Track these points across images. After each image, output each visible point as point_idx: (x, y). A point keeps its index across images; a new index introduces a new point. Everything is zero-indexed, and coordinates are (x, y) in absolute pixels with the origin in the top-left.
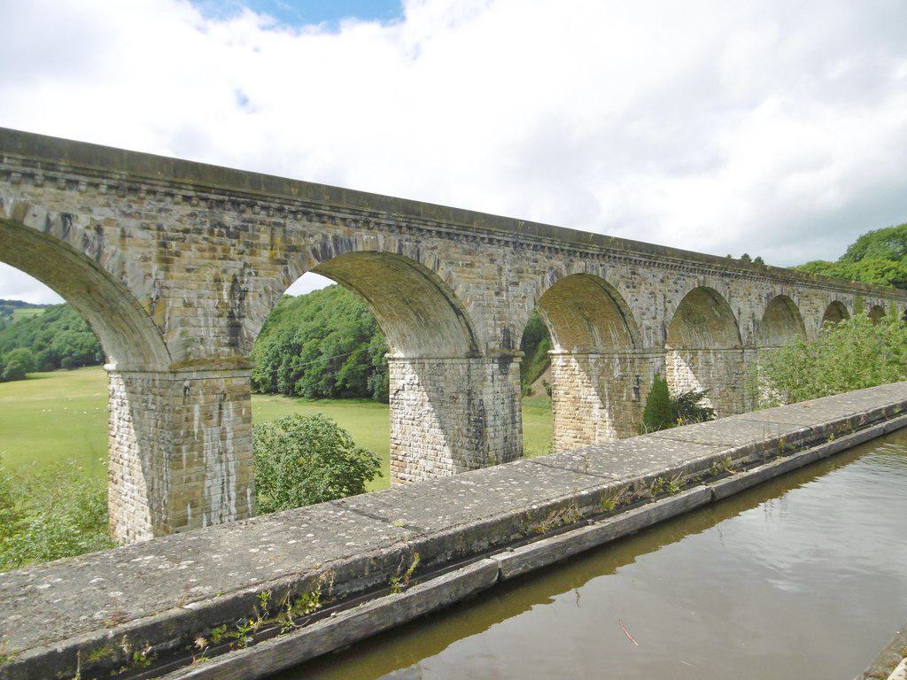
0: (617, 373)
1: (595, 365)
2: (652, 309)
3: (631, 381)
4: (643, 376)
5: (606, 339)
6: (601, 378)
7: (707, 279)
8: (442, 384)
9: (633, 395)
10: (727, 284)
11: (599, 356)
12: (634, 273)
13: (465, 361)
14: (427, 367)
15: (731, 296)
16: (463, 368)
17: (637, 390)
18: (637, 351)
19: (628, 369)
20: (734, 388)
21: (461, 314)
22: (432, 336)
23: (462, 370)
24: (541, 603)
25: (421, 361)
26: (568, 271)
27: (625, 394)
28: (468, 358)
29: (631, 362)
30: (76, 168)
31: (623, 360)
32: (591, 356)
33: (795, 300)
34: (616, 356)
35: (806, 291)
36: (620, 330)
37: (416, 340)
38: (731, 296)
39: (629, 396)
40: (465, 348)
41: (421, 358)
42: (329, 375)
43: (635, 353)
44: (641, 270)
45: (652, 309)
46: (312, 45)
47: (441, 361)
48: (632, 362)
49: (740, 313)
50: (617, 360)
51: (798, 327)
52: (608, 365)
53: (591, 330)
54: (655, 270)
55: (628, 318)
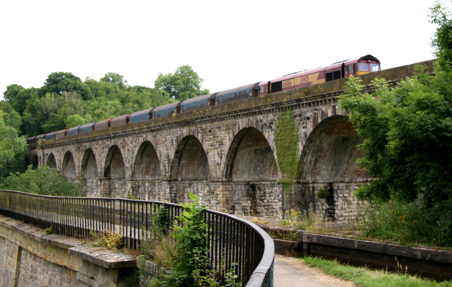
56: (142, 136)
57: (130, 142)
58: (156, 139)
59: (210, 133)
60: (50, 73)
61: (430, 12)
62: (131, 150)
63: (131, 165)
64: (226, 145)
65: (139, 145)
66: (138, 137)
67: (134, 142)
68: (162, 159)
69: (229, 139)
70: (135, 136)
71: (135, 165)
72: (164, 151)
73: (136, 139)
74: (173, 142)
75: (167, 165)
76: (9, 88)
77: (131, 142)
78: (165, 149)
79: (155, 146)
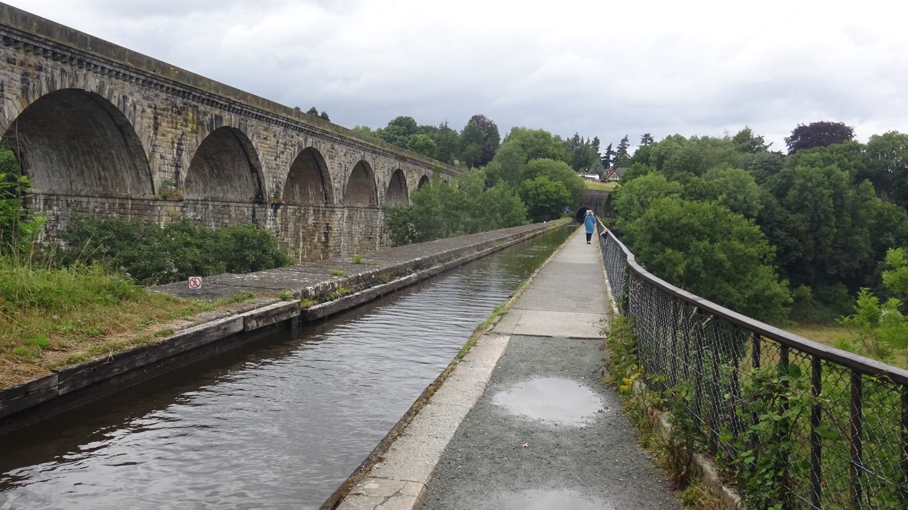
0: (311, 221)
1: (293, 214)
2: (339, 175)
3: (322, 228)
4: (332, 224)
5: (304, 195)
6: (297, 224)
7: (366, 154)
8: (227, 221)
9: (323, 238)
10: (374, 159)
11: (296, 207)
12: (333, 148)
13: (251, 205)
14: (211, 207)
15: (375, 169)
16: (248, 211)
17: (326, 235)
18: (329, 205)
19: (321, 218)
20: (370, 238)
21: (257, 172)
22: (220, 184)
23: (248, 212)
24: (94, 441)
25: (204, 202)
26: (305, 145)
27: (316, 237)
28: (254, 203)
29: (323, 213)
30: (166, 79)
31: (316, 212)
32: (289, 207)
33: (405, 173)
34: (311, 208)
35: (411, 166)
36: (317, 188)
37: (202, 186)
38: (375, 169)
39: (319, 239)
40: (251, 195)
41: (206, 200)
42: (818, 200)
43: (327, 207)
44: (336, 146)
45: (339, 175)
46: (817, 120)
47: (226, 204)
48: (324, 214)
49: (378, 182)
50: (312, 211)
51: (404, 194)
52: (304, 214)
53: (292, 187)
54: (343, 146)
55: (326, 180)
56: (360, 153)
57: (343, 154)
62: (343, 166)
63: (344, 186)
65: (356, 164)
66: (354, 151)
67: (349, 155)
73: (352, 154)
75: (383, 193)
77: (345, 155)
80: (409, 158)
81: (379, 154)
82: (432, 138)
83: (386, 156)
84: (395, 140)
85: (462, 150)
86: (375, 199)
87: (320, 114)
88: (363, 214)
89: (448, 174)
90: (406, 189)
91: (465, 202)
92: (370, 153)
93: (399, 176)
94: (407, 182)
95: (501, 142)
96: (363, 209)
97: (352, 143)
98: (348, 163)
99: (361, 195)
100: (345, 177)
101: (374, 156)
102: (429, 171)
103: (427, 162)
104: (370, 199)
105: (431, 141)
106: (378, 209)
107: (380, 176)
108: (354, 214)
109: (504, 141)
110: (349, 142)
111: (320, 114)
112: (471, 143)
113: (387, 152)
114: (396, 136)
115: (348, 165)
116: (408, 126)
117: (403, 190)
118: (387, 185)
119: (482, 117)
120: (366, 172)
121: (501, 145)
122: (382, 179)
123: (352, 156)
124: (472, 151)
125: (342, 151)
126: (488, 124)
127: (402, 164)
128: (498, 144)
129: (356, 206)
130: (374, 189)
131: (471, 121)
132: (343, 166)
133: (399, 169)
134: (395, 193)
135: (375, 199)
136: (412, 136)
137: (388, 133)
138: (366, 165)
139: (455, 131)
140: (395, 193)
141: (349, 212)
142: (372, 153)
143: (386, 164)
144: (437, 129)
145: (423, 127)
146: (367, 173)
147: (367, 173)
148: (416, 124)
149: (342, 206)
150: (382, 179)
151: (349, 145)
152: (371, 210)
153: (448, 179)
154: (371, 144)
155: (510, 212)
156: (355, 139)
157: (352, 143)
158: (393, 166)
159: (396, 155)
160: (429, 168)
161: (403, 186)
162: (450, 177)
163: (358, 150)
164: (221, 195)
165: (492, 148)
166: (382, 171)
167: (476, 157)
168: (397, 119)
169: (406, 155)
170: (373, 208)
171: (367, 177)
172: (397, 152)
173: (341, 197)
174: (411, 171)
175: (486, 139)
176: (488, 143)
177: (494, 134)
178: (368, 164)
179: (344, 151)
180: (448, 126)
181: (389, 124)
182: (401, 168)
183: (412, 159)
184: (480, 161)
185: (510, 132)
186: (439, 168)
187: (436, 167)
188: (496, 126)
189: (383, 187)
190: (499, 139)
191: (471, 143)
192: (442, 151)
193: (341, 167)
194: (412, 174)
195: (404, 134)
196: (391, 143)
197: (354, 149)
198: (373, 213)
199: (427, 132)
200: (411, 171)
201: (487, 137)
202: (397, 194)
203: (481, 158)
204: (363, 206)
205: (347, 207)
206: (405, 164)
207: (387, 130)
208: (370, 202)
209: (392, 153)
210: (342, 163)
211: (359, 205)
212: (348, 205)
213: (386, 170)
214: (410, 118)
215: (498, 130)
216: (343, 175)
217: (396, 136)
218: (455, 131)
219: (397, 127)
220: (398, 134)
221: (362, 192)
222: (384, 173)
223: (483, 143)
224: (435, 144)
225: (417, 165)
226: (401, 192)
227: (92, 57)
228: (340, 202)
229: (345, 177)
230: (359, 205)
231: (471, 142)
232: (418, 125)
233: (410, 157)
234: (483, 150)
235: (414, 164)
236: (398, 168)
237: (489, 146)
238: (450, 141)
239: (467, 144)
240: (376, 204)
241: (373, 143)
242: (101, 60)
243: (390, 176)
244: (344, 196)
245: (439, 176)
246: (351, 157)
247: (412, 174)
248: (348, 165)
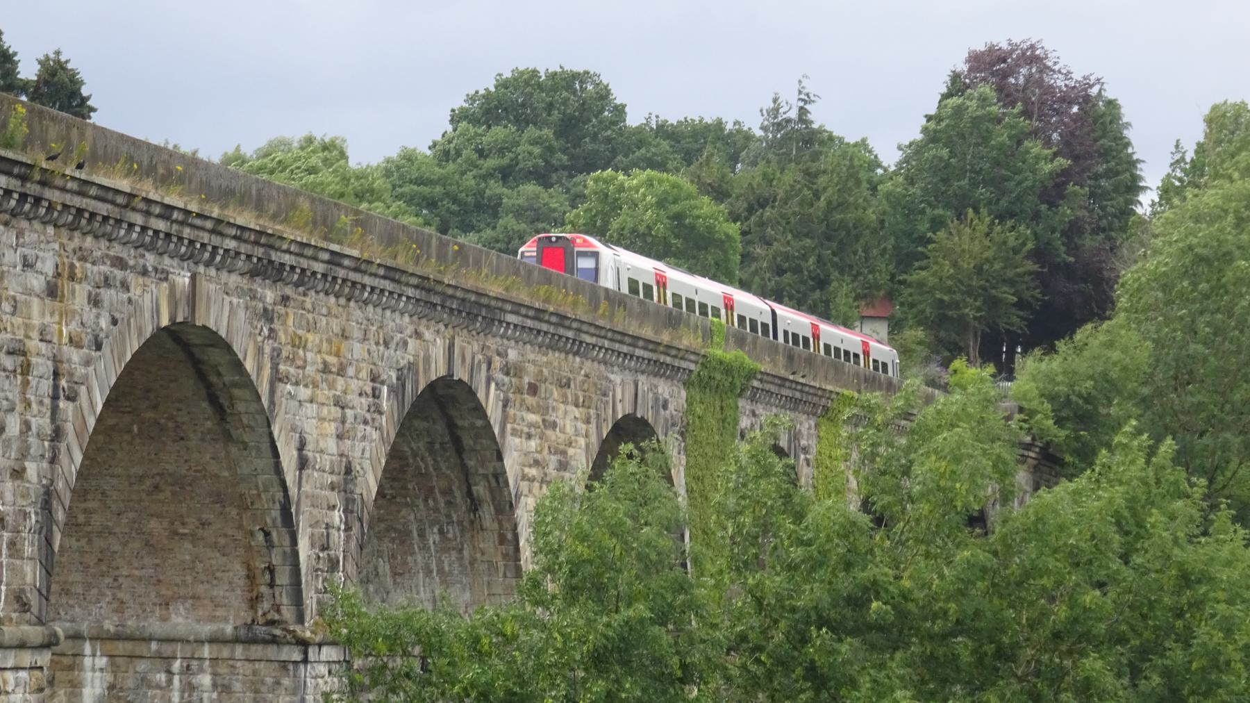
10: (267, 316)
15: (277, 378)
38: (277, 378)
49: (303, 464)
51: (488, 543)
54: (32, 233)
56: (164, 276)
57: (37, 283)
58: (272, 333)
59: (530, 400)
60: (1219, 100)
61: (924, 121)
62: (42, 366)
63: (47, 498)
64: (993, 533)
65: (133, 345)
66: (120, 263)
67: (81, 291)
68: (306, 488)
69: (587, 445)
70: (99, 248)
71: (80, 493)
72: (324, 436)
73: (107, 282)
74: (376, 395)
75: (338, 537)
76: (1215, 108)
77: (52, 291)
78: (331, 428)
79: (264, 390)
80: (517, 307)
81: (305, 280)
82: (719, 193)
83: (351, 292)
84: (492, 209)
85: (906, 260)
86: (283, 578)
87: (28, 70)
88: (206, 680)
89: (794, 404)
90: (505, 508)
91: (874, 589)
92: (234, 280)
93: (451, 426)
94: (511, 463)
95: (1146, 202)
96: (206, 651)
97: (103, 209)
98: (74, 342)
99: (185, 552)
100: (57, 435)
101: (270, 295)
102: (664, 388)
103: (647, 332)
104: (251, 577)
105: (706, 206)
106: (304, 644)
107: (310, 428)
108: (144, 682)
109: (1167, 191)
110: (78, 201)
111: (28, 70)
112: (960, 216)
113: (360, 266)
114: (495, 188)
115: (75, 356)
116: (570, 127)
117: (487, 514)
118: (368, 484)
119: (1032, 57)
120: (213, 399)
121: (1142, 222)
122: (331, 445)
123: (108, 295)
124: (967, 264)
125: (27, 264)
126: (1066, 100)
127: (469, 346)
128: (1126, 212)
129: (155, 626)
130: (276, 513)
131: (957, 85)
132: (42, 366)
133: (447, 382)
134: (433, 537)
135: (283, 578)
136: (590, 182)
137: (451, 166)
138: (215, 356)
139: (863, 144)
140: (433, 537)
141: (114, 667)
142: (253, 274)
143: (358, 350)
144: (748, 137)
145: (664, 131)
146: (221, 412)
147: (221, 412)
148: (620, 111)
149: (35, 633)
150: (325, 446)
151: (79, 221)
152: (257, 651)
153: (795, 436)
154: (245, 218)
155: (1185, 639)
156: (124, 185)
157: (103, 209)
158: (405, 359)
159: (424, 284)
160: (659, 370)
161: (480, 490)
162: (806, 425)
163: (150, 259)
164: (257, 666)
165: (1089, 242)
166: (324, 393)
167: (993, 303)
168: (503, 85)
169: (495, 289)
170: (274, 640)
171: (228, 438)
172: (429, 269)
173: (31, 573)
174: (533, 389)
175: (1054, 191)
176: (1067, 212)
177: (1105, 154)
178: (228, 348)
179: (49, 268)
180: (820, 117)
181: (457, 117)
182: (461, 374)
183: (539, 314)
184: (1016, 321)
185: (1194, 134)
186: (728, 369)
187: (705, 362)
188: (1111, 104)
189: (335, 498)
190: (1133, 187)
191: (960, 216)
192: (780, 272)
193: (26, 369)
194: (543, 410)
195: (542, 177)
196: (467, 228)
197: (117, 250)
198: (268, 673)
199: (689, 157)
200: (533, 389)
201: (1064, 176)
202: (445, 545)
203: (1021, 304)
204: (207, 629)
205: (100, 637)
206: (493, 343)
207: (445, 153)
208: (254, 602)
209: (392, 273)
210: (34, 344)
211: (181, 621)
212: (109, 626)
213: (354, 386)
214: (583, 77)
215: (1128, 134)
216: (41, 422)
217: (495, 188)
218: (863, 144)
219: (499, 132)
220: (506, 175)
221: (194, 538)
222: (339, 403)
223: (1036, 216)
224: (733, 229)
225: (578, 349)
226: (473, 526)
227: (597, 332)
228: (24, 607)
229: (57, 435)
230: (181, 621)
231: (961, 206)
232: (634, 119)
233: (523, 297)
234: (1038, 255)
235: (555, 344)
236: (438, 369)
237: (1073, 231)
238: (831, 208)
239: (937, 224)
240: (288, 613)
241: (259, 207)
242: (70, 185)
243: (388, 422)
244: (48, 563)
245: (727, 423)
246: (95, 302)
247: (543, 410)
248: (75, 356)
